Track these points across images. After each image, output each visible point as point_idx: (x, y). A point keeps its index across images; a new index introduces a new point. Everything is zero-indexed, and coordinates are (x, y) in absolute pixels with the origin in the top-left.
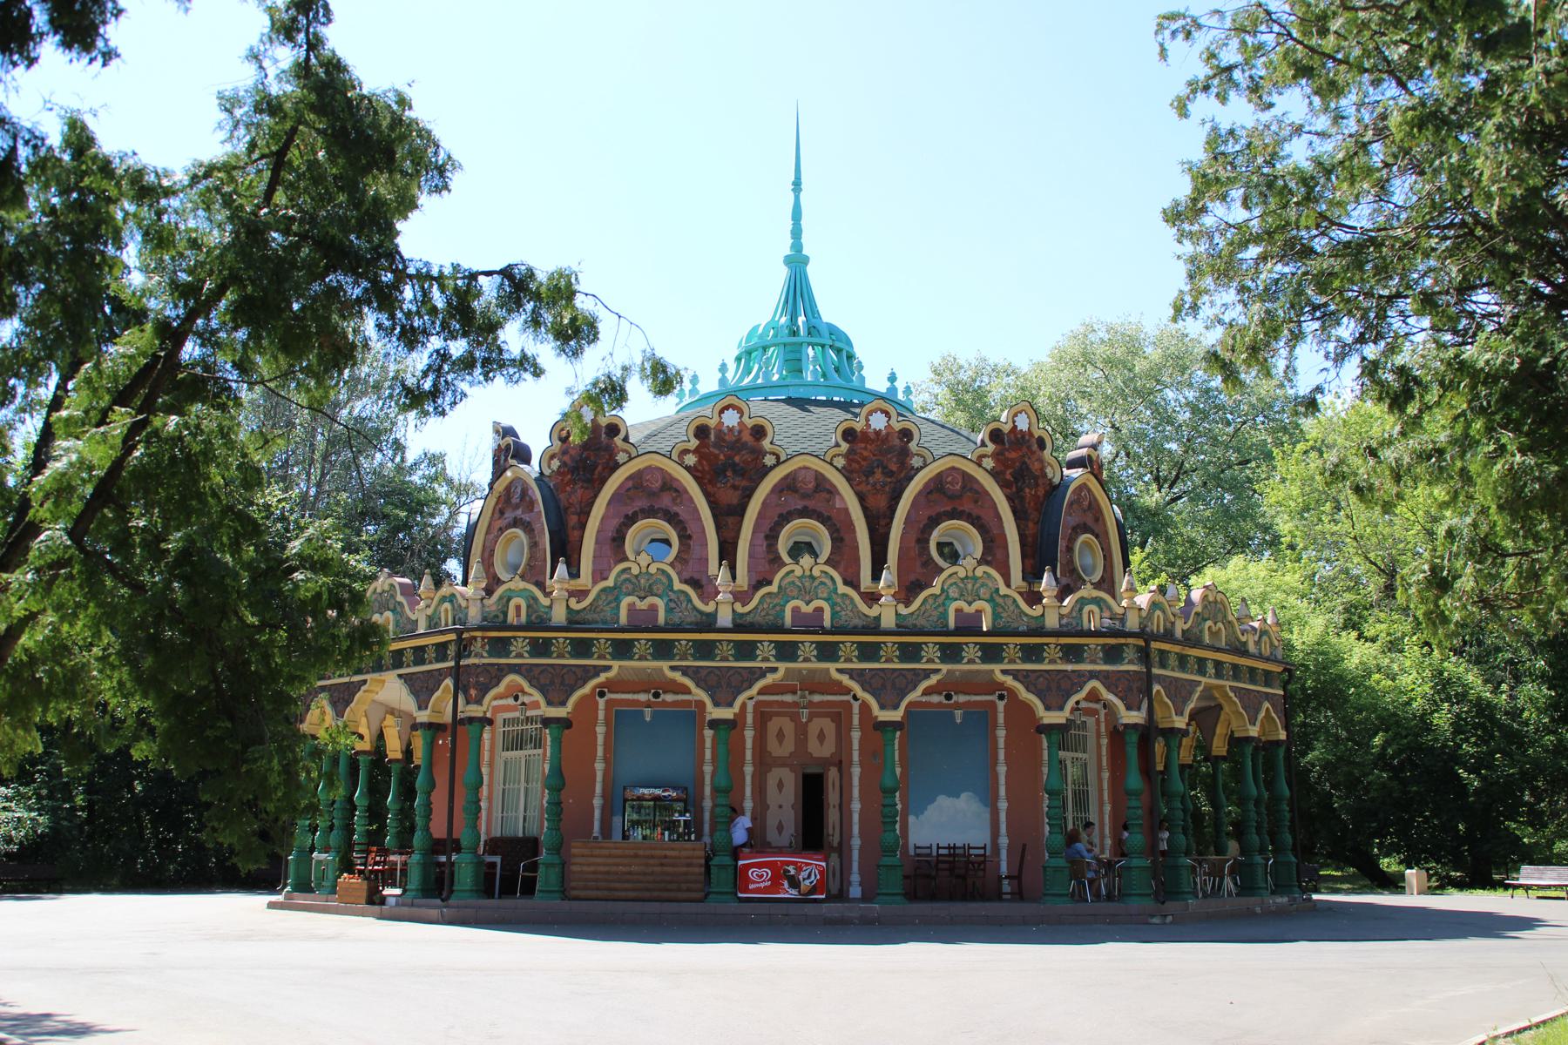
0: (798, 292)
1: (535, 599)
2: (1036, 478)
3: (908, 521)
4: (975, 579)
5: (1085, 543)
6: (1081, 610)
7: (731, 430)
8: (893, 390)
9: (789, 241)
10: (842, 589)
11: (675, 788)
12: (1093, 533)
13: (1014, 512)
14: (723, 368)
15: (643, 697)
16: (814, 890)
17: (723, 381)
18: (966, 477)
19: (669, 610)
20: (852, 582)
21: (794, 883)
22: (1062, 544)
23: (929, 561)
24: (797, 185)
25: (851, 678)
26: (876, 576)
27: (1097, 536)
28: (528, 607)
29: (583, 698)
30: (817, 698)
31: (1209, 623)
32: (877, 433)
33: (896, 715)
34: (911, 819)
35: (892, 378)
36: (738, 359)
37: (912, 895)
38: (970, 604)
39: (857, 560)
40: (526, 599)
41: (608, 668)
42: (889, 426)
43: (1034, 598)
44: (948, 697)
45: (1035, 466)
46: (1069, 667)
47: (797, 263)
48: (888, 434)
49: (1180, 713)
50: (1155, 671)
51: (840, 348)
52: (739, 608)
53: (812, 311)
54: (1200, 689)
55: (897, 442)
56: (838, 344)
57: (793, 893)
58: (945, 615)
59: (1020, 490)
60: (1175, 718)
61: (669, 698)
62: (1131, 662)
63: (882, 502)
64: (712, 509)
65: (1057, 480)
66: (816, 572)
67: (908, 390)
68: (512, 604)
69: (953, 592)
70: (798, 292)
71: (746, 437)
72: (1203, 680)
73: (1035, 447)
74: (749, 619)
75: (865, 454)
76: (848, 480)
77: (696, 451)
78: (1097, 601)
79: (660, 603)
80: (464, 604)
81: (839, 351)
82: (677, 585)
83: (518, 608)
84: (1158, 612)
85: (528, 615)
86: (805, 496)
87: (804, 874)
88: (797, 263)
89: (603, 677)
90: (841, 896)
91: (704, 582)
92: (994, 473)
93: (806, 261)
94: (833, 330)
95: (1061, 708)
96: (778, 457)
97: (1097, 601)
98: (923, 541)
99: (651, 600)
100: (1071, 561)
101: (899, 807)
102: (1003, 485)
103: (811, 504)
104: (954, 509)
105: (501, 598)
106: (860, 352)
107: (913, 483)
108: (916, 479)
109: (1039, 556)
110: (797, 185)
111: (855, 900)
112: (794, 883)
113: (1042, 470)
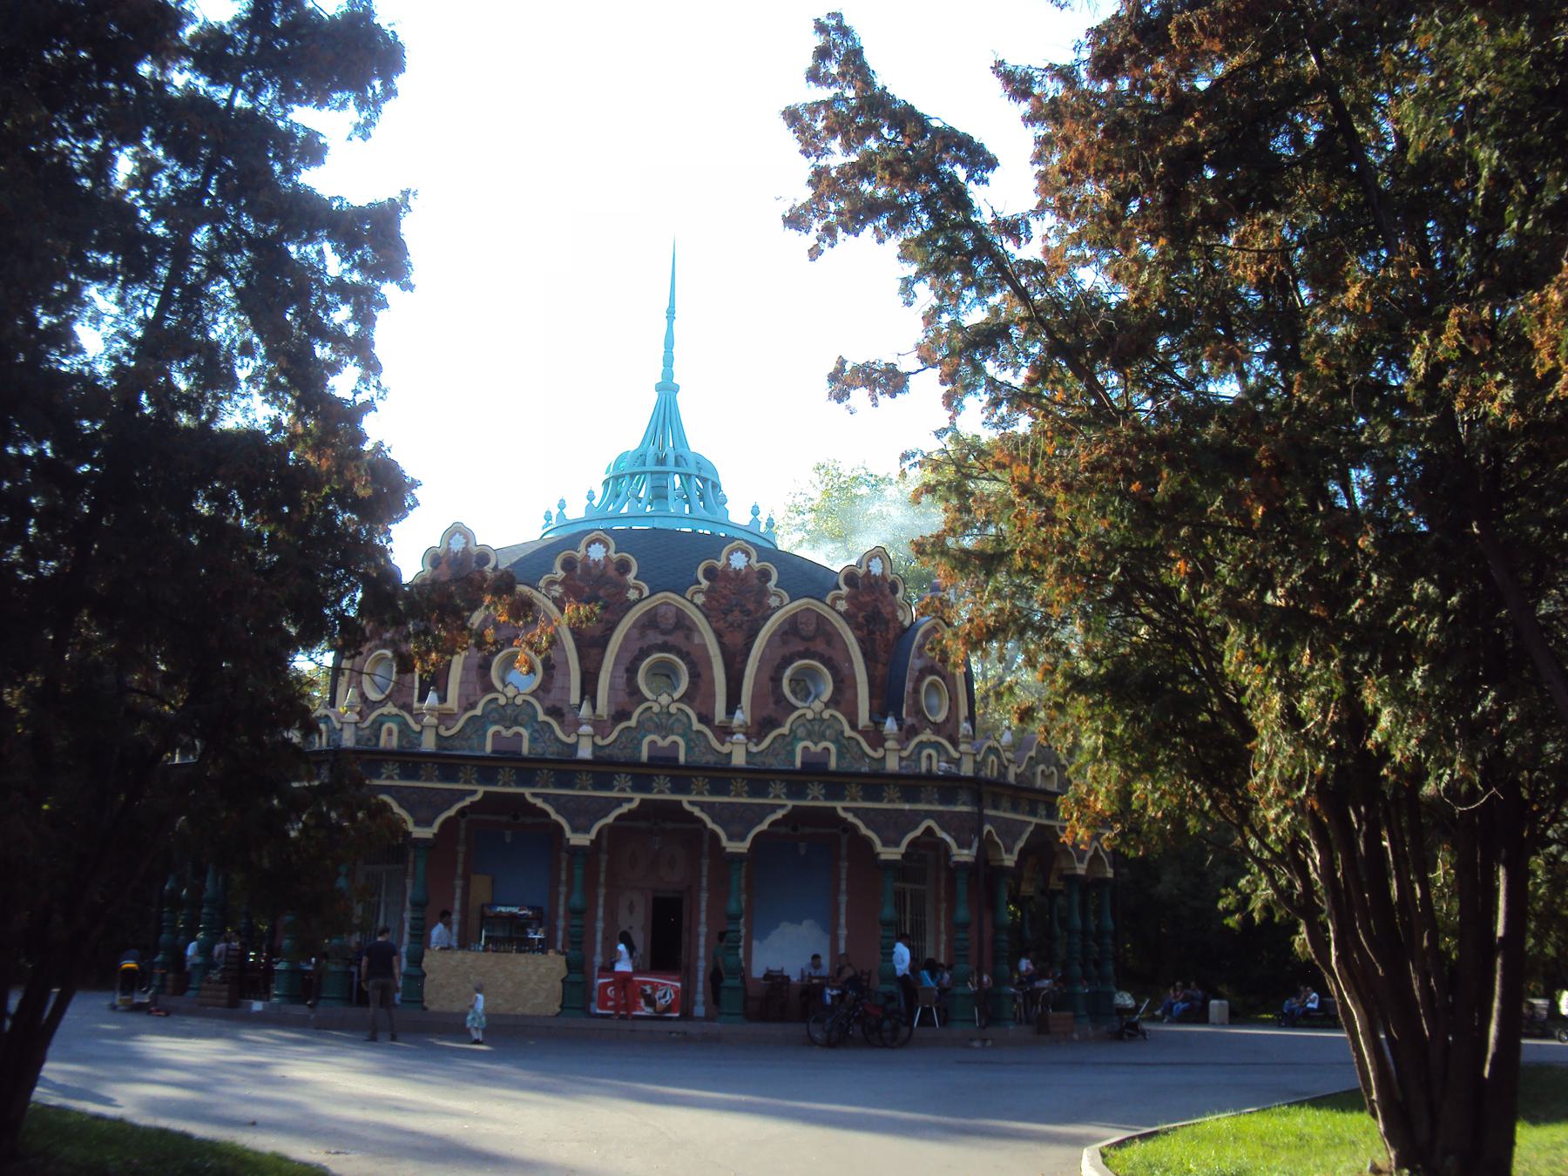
0: (666, 418)
1: (406, 724)
2: (887, 623)
3: (762, 660)
4: (822, 720)
5: (933, 685)
6: (919, 753)
7: (597, 563)
8: (756, 522)
9: (660, 367)
10: (696, 726)
11: (530, 908)
12: (939, 674)
13: (865, 654)
14: (591, 496)
15: (504, 819)
16: (669, 1008)
17: (589, 507)
18: (821, 620)
19: (533, 740)
20: (706, 719)
21: (651, 1001)
22: (909, 686)
23: (780, 699)
24: (671, 314)
25: (702, 810)
26: (731, 708)
27: (943, 678)
28: (400, 732)
29: (449, 819)
30: (669, 825)
31: (1042, 767)
32: (738, 572)
33: (742, 847)
34: (755, 943)
35: (755, 511)
36: (606, 483)
37: (750, 1016)
38: (816, 744)
39: (713, 695)
40: (399, 725)
41: (630, 800)
42: (748, 566)
43: (877, 739)
44: (795, 829)
45: (886, 610)
46: (907, 807)
47: (667, 388)
48: (747, 574)
49: (1009, 850)
50: (989, 812)
51: (705, 482)
52: (754, 749)
53: (681, 438)
54: (1031, 828)
55: (756, 581)
56: (703, 474)
57: (648, 1011)
58: (792, 753)
59: (871, 633)
60: (1005, 856)
61: (529, 820)
62: (964, 804)
63: (738, 638)
64: (576, 640)
65: (907, 623)
66: (673, 709)
67: (770, 523)
68: (384, 728)
69: (801, 732)
70: (666, 418)
71: (612, 572)
72: (1034, 820)
73: (888, 591)
74: (607, 751)
75: (726, 592)
76: (707, 617)
77: (563, 583)
78: (937, 746)
79: (525, 732)
80: (338, 726)
81: (704, 480)
82: (542, 717)
83: (390, 733)
84: (992, 757)
85: (400, 739)
86: (664, 633)
87: (659, 994)
88: (667, 388)
89: (468, 801)
90: (687, 1015)
91: (566, 710)
92: (846, 616)
93: (676, 389)
94: (701, 463)
95: (897, 844)
96: (641, 593)
97: (937, 746)
98: (776, 680)
99: (516, 729)
100: (917, 702)
101: (743, 932)
102: (856, 627)
103: (670, 639)
104: (807, 650)
105: (373, 722)
106: (727, 488)
107: (769, 623)
108: (774, 618)
109: (887, 698)
110: (671, 314)
111: (700, 1019)
112: (651, 1001)
113: (894, 613)
